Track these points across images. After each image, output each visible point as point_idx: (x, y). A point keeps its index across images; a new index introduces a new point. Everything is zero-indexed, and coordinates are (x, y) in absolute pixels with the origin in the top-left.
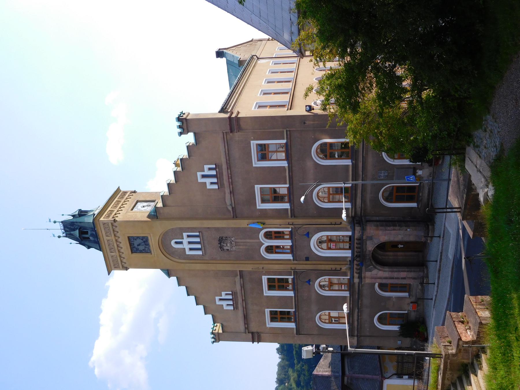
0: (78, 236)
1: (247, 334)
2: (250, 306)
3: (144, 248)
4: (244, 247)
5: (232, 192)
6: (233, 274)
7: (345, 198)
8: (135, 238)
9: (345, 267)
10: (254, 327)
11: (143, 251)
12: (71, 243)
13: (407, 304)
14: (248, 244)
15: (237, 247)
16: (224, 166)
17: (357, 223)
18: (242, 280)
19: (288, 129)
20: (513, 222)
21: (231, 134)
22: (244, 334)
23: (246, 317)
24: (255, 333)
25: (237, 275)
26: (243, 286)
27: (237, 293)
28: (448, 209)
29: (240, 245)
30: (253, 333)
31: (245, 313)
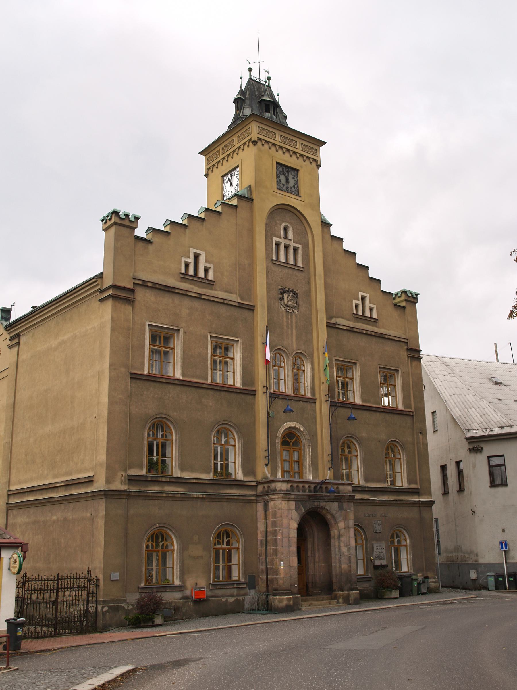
0: (263, 99)
1: (132, 279)
2: (187, 302)
3: (282, 183)
4: (285, 323)
5: (351, 330)
8: (278, 173)
9: (268, 472)
10: (141, 295)
11: (278, 179)
12: (241, 78)
13: (196, 583)
14: (290, 332)
15: (285, 314)
16: (376, 330)
17: (291, 486)
18: (236, 304)
19: (414, 413)
21: (406, 347)
22: (131, 275)
24: (133, 295)
25: (242, 299)
26: (224, 303)
27: (212, 289)
28: (227, 601)
29: (287, 318)
30: (133, 291)
31: (177, 291)
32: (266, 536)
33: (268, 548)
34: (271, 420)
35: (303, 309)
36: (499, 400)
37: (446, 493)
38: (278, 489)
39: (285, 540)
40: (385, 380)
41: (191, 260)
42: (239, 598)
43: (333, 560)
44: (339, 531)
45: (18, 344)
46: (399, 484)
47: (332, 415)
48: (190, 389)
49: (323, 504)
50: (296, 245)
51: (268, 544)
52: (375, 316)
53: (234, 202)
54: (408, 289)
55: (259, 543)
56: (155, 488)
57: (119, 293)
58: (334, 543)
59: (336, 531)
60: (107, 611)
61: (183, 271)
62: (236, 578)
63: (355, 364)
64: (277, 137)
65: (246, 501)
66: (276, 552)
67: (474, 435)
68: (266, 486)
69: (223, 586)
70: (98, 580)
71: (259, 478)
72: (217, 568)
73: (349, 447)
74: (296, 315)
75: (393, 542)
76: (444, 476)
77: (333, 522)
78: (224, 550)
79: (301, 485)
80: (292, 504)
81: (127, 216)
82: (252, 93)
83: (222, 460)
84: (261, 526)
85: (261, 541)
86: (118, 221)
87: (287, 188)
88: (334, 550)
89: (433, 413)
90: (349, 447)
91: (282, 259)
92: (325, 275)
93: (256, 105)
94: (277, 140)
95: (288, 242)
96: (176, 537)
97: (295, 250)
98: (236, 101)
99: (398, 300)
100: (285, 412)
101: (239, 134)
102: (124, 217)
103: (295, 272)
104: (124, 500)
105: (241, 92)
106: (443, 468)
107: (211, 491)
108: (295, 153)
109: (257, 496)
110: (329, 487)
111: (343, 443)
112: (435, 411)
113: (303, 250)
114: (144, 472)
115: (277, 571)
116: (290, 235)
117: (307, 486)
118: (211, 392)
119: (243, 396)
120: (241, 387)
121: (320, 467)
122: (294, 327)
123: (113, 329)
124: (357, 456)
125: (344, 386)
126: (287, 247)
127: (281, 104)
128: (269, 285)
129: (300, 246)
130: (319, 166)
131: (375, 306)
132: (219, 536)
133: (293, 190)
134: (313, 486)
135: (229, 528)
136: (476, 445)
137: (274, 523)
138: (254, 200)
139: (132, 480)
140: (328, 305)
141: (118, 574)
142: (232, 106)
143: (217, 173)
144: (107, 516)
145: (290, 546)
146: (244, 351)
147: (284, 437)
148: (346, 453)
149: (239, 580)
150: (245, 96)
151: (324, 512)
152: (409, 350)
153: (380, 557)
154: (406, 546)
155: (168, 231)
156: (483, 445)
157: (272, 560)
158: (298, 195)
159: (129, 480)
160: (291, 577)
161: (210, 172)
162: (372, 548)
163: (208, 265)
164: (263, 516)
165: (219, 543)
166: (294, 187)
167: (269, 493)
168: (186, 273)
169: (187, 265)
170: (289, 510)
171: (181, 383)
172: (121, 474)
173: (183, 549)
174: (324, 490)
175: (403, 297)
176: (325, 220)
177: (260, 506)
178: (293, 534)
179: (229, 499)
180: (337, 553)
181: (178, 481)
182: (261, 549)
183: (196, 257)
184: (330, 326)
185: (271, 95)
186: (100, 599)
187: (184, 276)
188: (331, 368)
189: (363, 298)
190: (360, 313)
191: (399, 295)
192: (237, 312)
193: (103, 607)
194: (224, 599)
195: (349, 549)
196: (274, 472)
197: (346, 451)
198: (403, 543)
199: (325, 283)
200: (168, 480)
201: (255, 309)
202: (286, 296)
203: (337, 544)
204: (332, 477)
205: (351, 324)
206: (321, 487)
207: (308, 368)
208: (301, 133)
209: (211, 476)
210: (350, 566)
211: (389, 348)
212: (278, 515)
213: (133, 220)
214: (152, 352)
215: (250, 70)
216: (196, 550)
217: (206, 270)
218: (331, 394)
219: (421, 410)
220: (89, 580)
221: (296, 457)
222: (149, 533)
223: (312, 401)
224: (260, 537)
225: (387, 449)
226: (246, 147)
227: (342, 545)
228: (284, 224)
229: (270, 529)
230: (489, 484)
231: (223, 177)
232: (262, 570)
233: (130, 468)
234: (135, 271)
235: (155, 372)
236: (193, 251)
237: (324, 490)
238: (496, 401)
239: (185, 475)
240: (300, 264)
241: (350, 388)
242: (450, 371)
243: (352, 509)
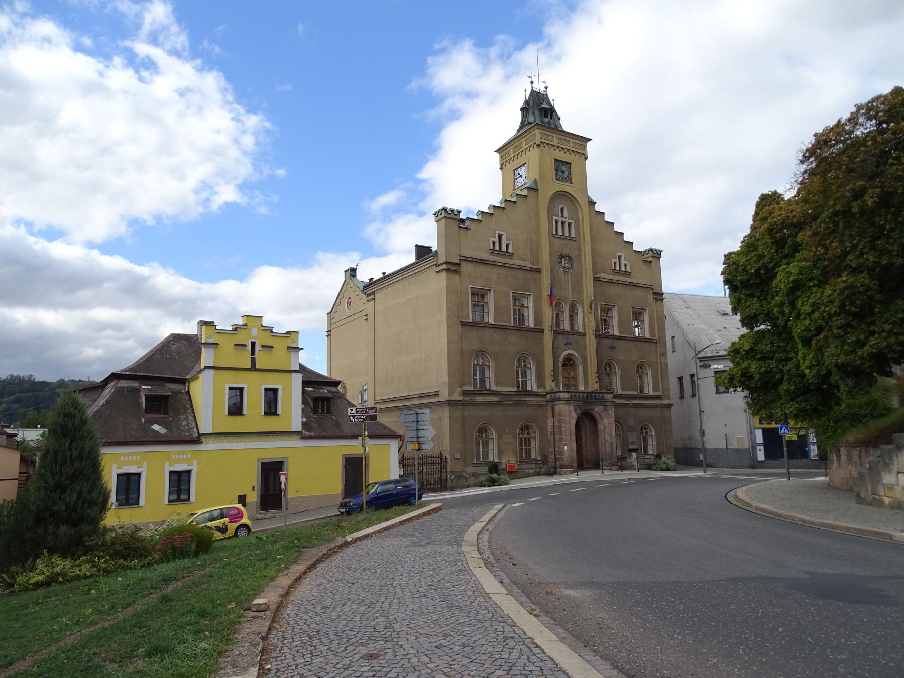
4: (563, 280)
5: (611, 282)
6: (536, 258)
7: (8, 427)
10: (466, 268)
12: (526, 91)
14: (567, 285)
15: (563, 272)
16: (629, 280)
17: (571, 395)
18: (529, 269)
20: (647, 466)
22: (458, 253)
23: (482, 262)
25: (533, 265)
26: (521, 268)
27: (512, 259)
29: (565, 276)
30: (459, 265)
31: (488, 262)
32: (554, 429)
33: (556, 437)
34: (555, 349)
35: (576, 268)
36: (725, 328)
37: (682, 397)
38: (562, 397)
39: (568, 432)
40: (636, 317)
41: (497, 239)
42: (536, 470)
43: (600, 446)
44: (604, 425)
45: (374, 299)
46: (646, 392)
47: (598, 344)
48: (500, 330)
49: (592, 407)
50: (570, 221)
51: (556, 434)
52: (628, 270)
53: (525, 193)
54: (654, 247)
55: (549, 433)
56: (480, 398)
57: (450, 267)
58: (601, 434)
59: (602, 426)
60: (454, 478)
61: (492, 248)
62: (535, 457)
63: (614, 306)
64: (555, 139)
65: (539, 405)
66: (561, 440)
67: (704, 355)
68: (553, 395)
69: (526, 462)
70: (447, 458)
71: (548, 390)
72: (521, 451)
73: (610, 366)
74: (571, 274)
75: (642, 433)
76: (681, 385)
77: (600, 419)
78: (525, 439)
79: (577, 394)
80: (572, 408)
81: (452, 211)
82: (534, 103)
83: (522, 378)
84: (550, 423)
85: (551, 433)
86: (447, 216)
87: (563, 178)
88: (601, 439)
89: (673, 337)
90: (610, 366)
91: (560, 233)
92: (592, 242)
93: (537, 112)
94: (555, 142)
95: (564, 220)
96: (494, 430)
97: (569, 225)
98: (522, 110)
99: (646, 256)
100: (565, 344)
101: (526, 138)
102: (450, 212)
103: (570, 241)
104: (460, 407)
105: (527, 102)
106: (680, 379)
107: (516, 399)
108: (568, 150)
109: (546, 402)
110: (597, 395)
111: (606, 364)
112: (674, 337)
113: (575, 225)
115: (562, 453)
116: (565, 214)
117: (581, 395)
118: (514, 332)
119: (535, 334)
120: (534, 327)
121: (590, 381)
122: (570, 283)
123: (447, 293)
124: (616, 372)
125: (605, 322)
126: (563, 223)
127: (555, 108)
128: (551, 253)
129: (573, 222)
131: (628, 263)
132: (522, 429)
133: (567, 179)
134: (585, 395)
135: (529, 424)
136: (705, 363)
137: (560, 421)
138: (539, 191)
139: (465, 393)
140: (594, 264)
141: (459, 454)
142: (519, 114)
143: (510, 167)
144: (450, 417)
145: (570, 436)
146: (535, 302)
147: (564, 361)
148: (608, 370)
149: (536, 458)
150: (529, 106)
151: (593, 412)
152: (655, 294)
153: (633, 443)
154: (652, 436)
155: (480, 219)
156: (710, 363)
157: (559, 445)
158: (571, 183)
159: (463, 393)
160: (571, 456)
161: (504, 166)
162: (627, 438)
163: (508, 242)
164: (551, 415)
165: (522, 434)
166: (568, 177)
167: (555, 400)
168: (494, 249)
169: (494, 243)
170: (569, 411)
171: (494, 327)
173: (500, 437)
174: (593, 398)
175: (651, 253)
176: (591, 199)
177: (549, 409)
178: (573, 428)
179: (524, 404)
180: (603, 440)
181: (494, 393)
182: (550, 438)
183: (500, 236)
184: (596, 280)
185: (549, 103)
186: (449, 469)
188: (596, 309)
189: (620, 257)
190: (618, 268)
191: (647, 252)
192: (529, 274)
193: (451, 475)
194: (527, 471)
195: (611, 438)
196: (558, 385)
197: (608, 369)
198: (650, 434)
199: (592, 248)
200: (488, 392)
201: (542, 271)
202: (563, 260)
203: (603, 434)
204: (598, 389)
205: (611, 277)
206: (591, 396)
207: (580, 311)
208: (572, 134)
209: (515, 389)
210: (612, 450)
211: (639, 293)
212: (563, 415)
213: (457, 214)
214: (473, 306)
215: (532, 83)
216: (508, 439)
217: (507, 246)
218: (597, 330)
219: (663, 337)
220: (442, 459)
221: (572, 375)
222: (477, 428)
223: (583, 335)
224: (549, 429)
225: (638, 367)
226: (532, 148)
227: (606, 434)
228: (561, 206)
229: (556, 424)
230: (715, 392)
231: (514, 170)
232: (552, 452)
233: (463, 384)
234: (460, 251)
235: (477, 319)
236: (498, 232)
237: (593, 398)
238: (722, 329)
239: (499, 389)
240: (573, 235)
241: (610, 324)
242: (686, 306)
243: (613, 410)
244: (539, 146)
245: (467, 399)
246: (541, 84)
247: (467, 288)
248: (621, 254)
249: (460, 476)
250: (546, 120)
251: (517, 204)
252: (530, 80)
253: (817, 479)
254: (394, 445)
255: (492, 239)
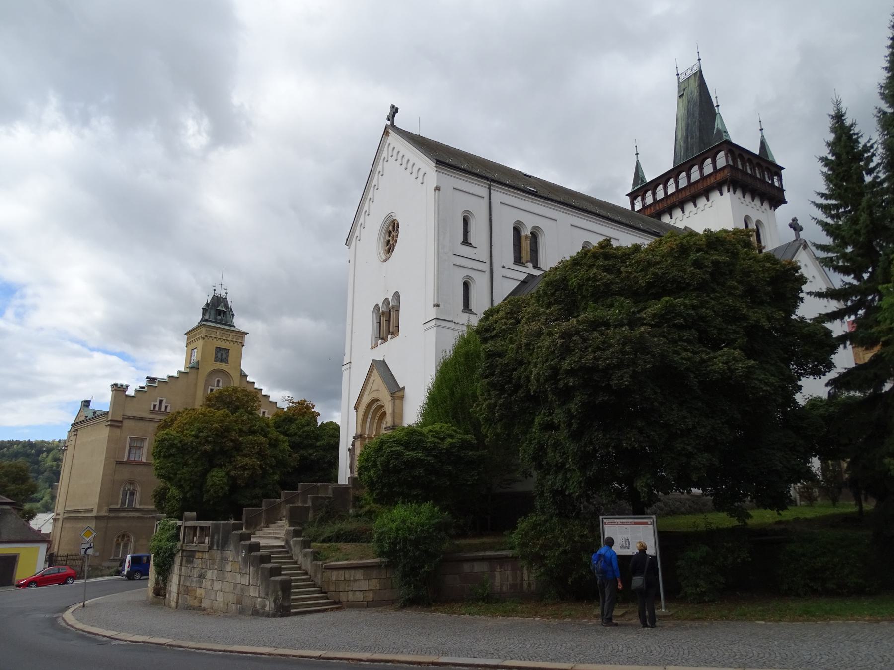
10: (126, 423)
22: (122, 414)
23: (142, 419)
41: (158, 403)
45: (77, 435)
56: (124, 514)
61: (152, 409)
64: (218, 333)
93: (213, 312)
105: (207, 304)
114: (119, 506)
130: (243, 346)
139: (111, 510)
143: (192, 346)
169: (155, 406)
171: (144, 464)
172: (106, 508)
183: (161, 401)
187: (153, 412)
215: (215, 290)
217: (166, 407)
228: (216, 380)
233: (112, 504)
235: (132, 459)
239: (141, 507)
244: (203, 339)
245: (112, 514)
246: (223, 290)
247: (127, 437)
248: (264, 411)
249: (97, 569)
250: (219, 317)
251: (189, 374)
252: (214, 288)
253: (659, 566)
254: (43, 548)
255: (153, 404)
